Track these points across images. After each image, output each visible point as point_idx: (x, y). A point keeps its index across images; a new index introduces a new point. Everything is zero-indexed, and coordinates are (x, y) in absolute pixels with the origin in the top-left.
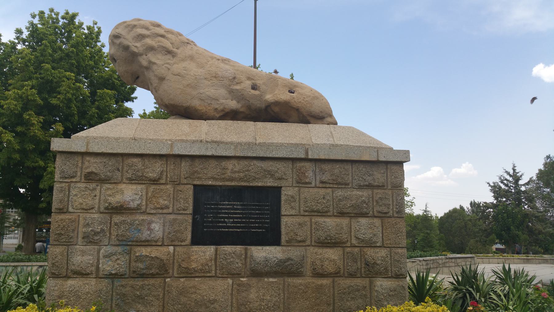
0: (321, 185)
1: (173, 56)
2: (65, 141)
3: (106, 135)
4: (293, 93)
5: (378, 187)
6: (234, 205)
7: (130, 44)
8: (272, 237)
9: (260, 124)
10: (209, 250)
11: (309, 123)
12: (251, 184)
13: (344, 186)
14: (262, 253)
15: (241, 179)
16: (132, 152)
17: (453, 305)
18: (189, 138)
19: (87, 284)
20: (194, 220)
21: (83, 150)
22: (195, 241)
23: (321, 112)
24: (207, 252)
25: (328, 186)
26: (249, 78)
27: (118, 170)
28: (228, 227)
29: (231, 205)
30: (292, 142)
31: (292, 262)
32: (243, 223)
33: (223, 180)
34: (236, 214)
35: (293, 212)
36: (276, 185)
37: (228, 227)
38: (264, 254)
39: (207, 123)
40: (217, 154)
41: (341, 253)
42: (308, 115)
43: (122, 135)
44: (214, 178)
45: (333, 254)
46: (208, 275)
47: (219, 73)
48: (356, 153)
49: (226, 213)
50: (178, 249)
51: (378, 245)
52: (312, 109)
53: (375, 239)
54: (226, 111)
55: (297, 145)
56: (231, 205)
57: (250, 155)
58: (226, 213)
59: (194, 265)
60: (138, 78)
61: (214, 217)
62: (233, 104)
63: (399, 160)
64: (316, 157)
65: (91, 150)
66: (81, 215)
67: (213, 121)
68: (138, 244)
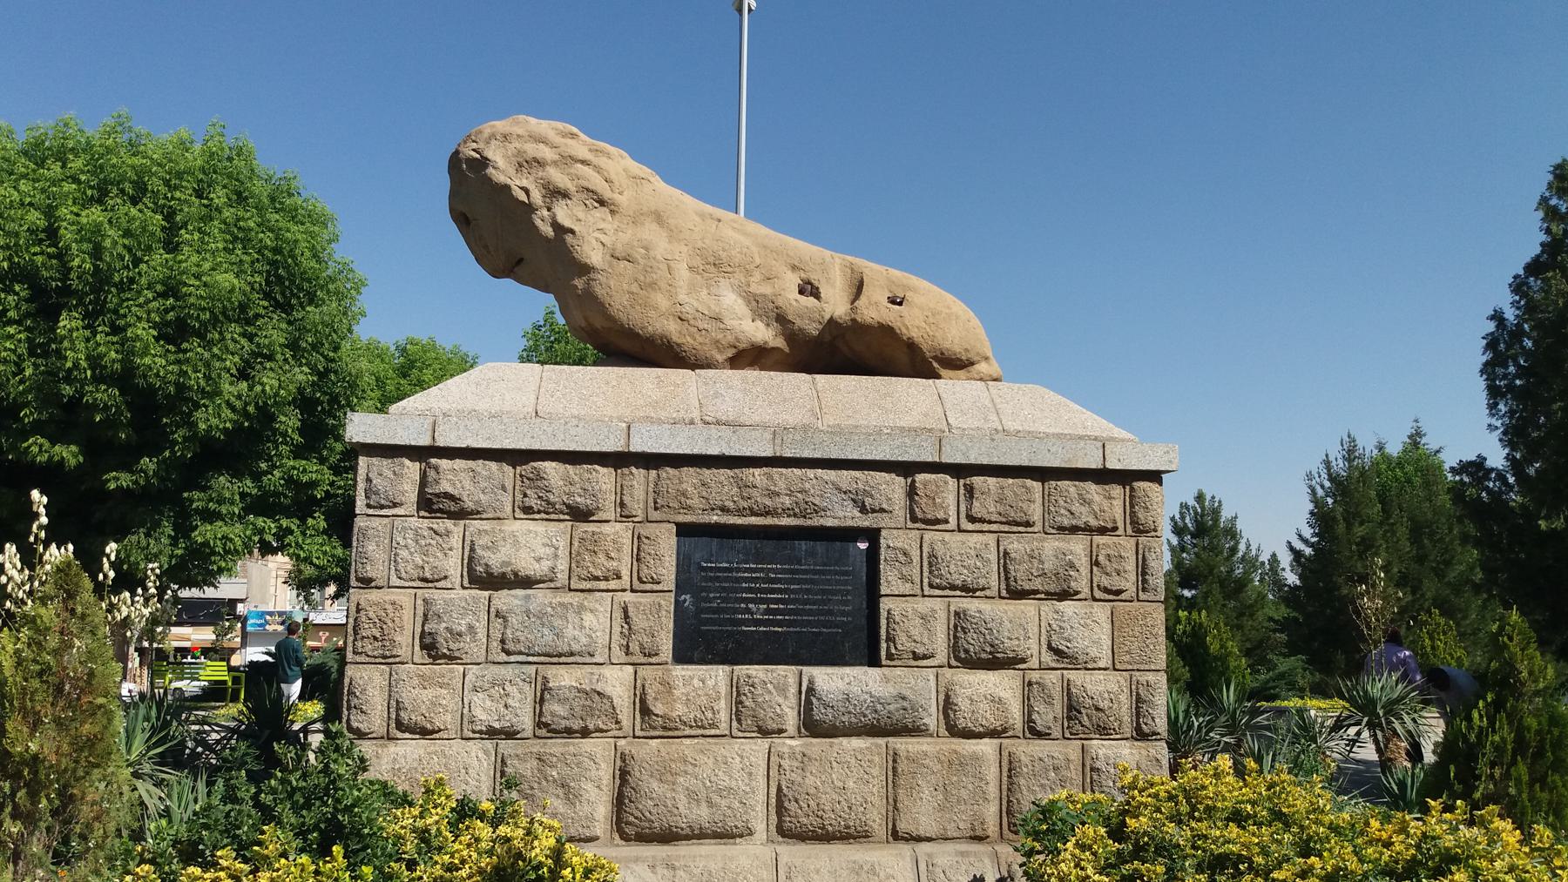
0: (970, 527)
1: (612, 212)
2: (379, 418)
3: (469, 407)
4: (900, 304)
5: (1102, 531)
6: (770, 570)
7: (509, 182)
8: (864, 642)
9: (821, 379)
10: (717, 676)
11: (938, 377)
12: (809, 523)
13: (1021, 529)
14: (837, 682)
15: (787, 511)
16: (536, 446)
17: (733, 836)
18: (663, 415)
19: (435, 753)
20: (678, 604)
21: (425, 441)
22: (683, 655)
23: (967, 350)
24: (709, 682)
25: (986, 527)
26: (794, 268)
27: (504, 488)
28: (758, 623)
29: (762, 570)
30: (902, 424)
31: (905, 704)
32: (790, 612)
33: (740, 512)
34: (773, 591)
35: (906, 588)
36: (866, 524)
37: (758, 623)
38: (841, 685)
39: (744, 380)
40: (733, 453)
41: (1019, 682)
42: (935, 358)
43: (507, 408)
44: (724, 510)
45: (1001, 685)
46: (713, 732)
47: (723, 255)
48: (1053, 450)
49: (750, 590)
50: (642, 671)
51: (1102, 664)
52: (946, 345)
53: (1093, 652)
54: (742, 346)
55: (915, 432)
56: (762, 570)
57: (807, 454)
58: (750, 590)
59: (680, 710)
60: (520, 261)
61: (724, 600)
62: (763, 333)
63: (1152, 467)
64: (959, 459)
65: (441, 443)
66: (420, 592)
67: (711, 372)
68: (555, 660)
